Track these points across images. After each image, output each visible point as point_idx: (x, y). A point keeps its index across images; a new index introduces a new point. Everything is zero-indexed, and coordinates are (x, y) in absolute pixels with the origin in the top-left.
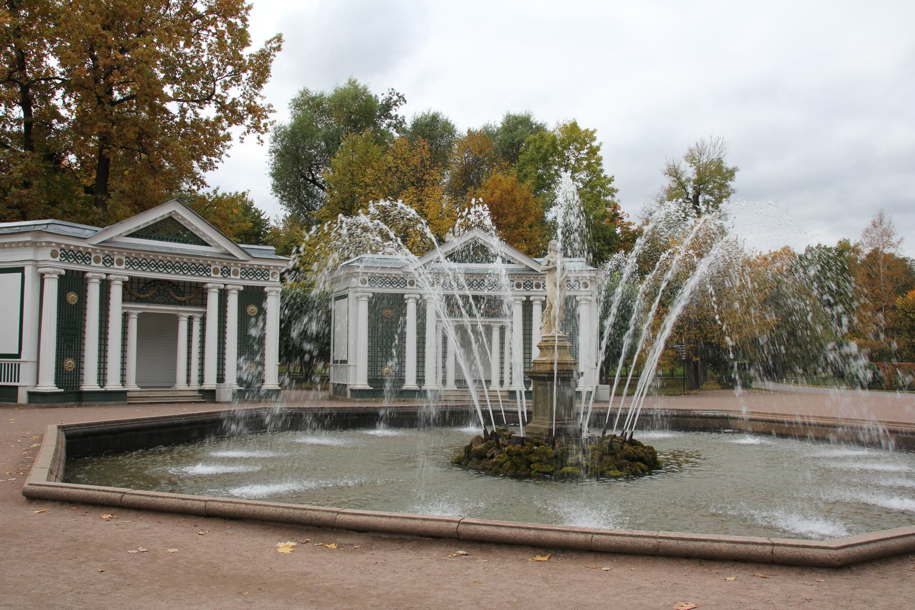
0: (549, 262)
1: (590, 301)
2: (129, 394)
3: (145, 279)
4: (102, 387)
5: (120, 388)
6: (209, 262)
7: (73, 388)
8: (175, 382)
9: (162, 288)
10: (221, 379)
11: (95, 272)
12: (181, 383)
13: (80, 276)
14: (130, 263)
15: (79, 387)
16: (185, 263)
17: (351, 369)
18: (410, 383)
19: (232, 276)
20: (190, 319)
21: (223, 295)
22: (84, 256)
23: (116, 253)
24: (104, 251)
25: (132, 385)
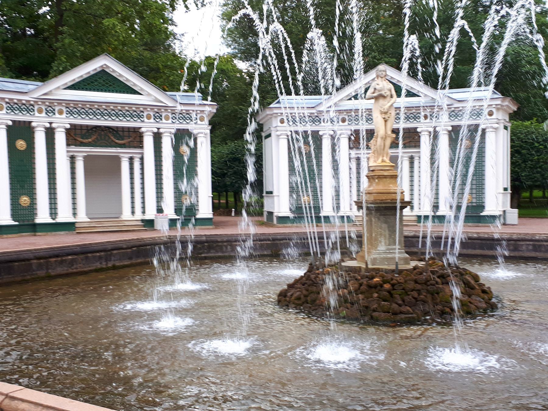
0: (375, 89)
1: (496, 129)
2: (77, 225)
3: (87, 126)
4: (54, 219)
5: (72, 220)
6: (141, 109)
7: (28, 220)
8: (121, 213)
9: (103, 133)
10: (160, 210)
11: (325, 130)
12: (126, 215)
13: (27, 125)
14: (70, 113)
15: (33, 220)
16: (317, 116)
17: (276, 198)
18: (327, 210)
19: (164, 121)
20: (131, 159)
21: (157, 137)
22: (28, 107)
23: (163, 110)
24: (44, 102)
25: (82, 217)
